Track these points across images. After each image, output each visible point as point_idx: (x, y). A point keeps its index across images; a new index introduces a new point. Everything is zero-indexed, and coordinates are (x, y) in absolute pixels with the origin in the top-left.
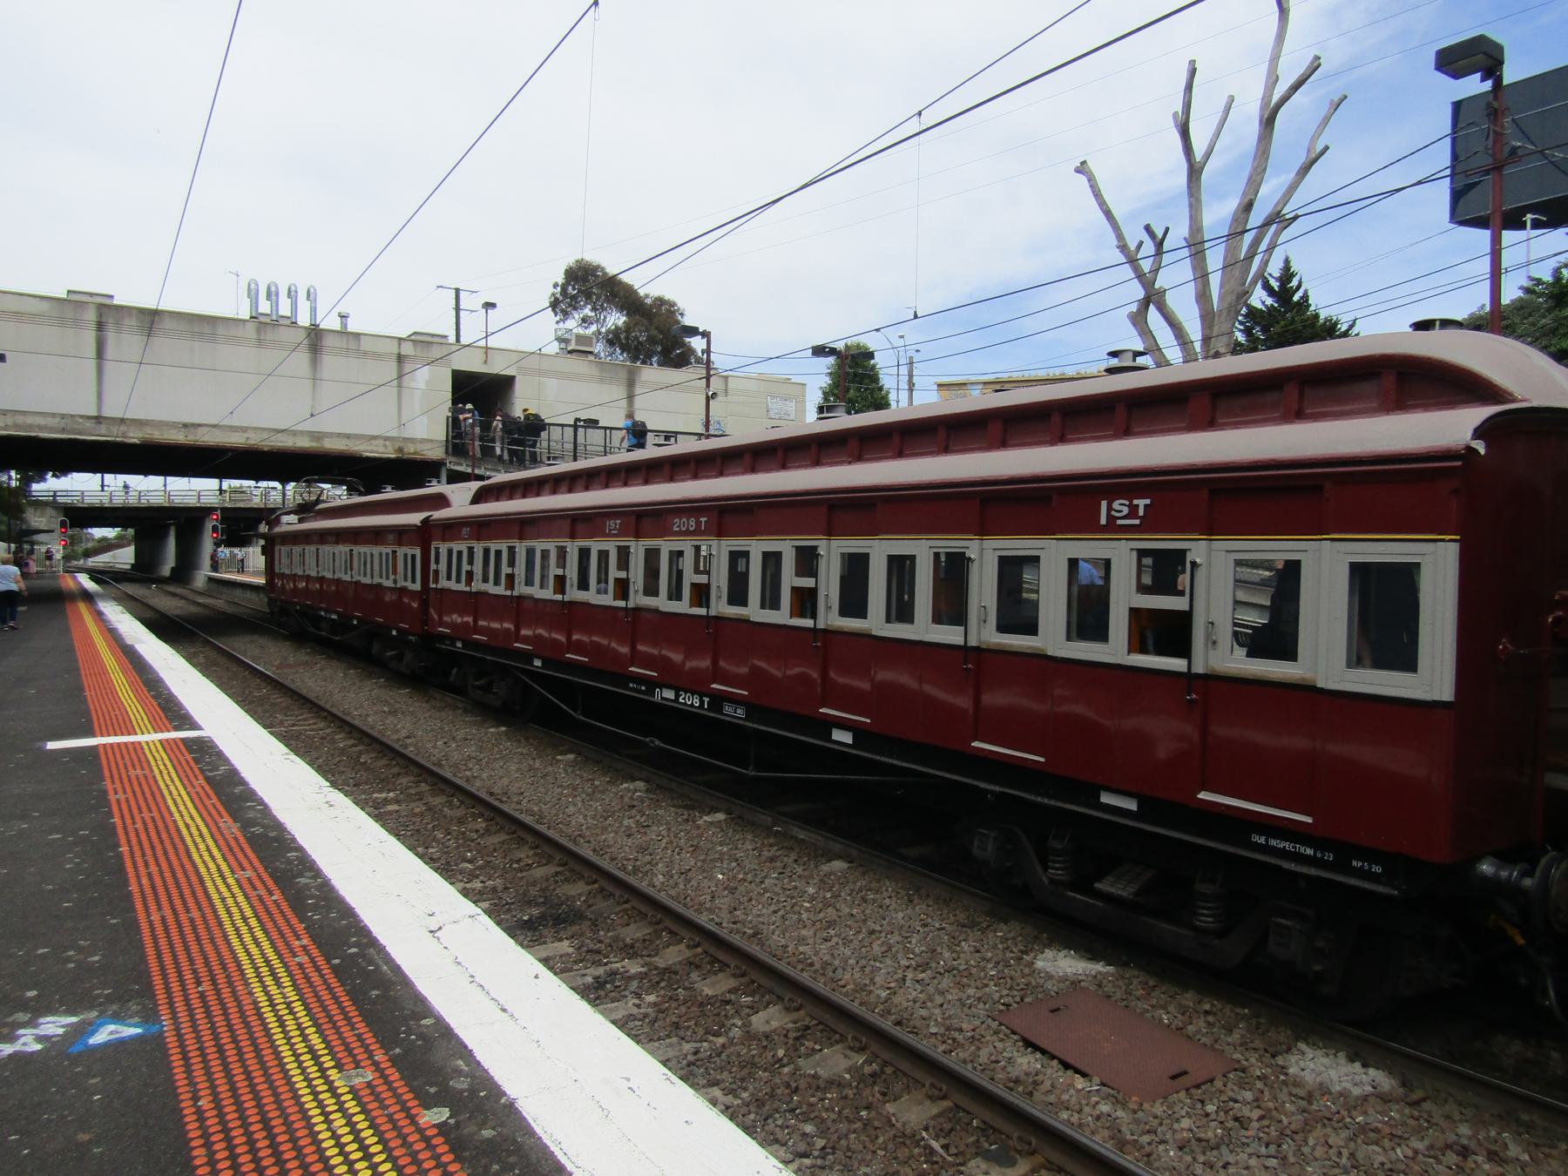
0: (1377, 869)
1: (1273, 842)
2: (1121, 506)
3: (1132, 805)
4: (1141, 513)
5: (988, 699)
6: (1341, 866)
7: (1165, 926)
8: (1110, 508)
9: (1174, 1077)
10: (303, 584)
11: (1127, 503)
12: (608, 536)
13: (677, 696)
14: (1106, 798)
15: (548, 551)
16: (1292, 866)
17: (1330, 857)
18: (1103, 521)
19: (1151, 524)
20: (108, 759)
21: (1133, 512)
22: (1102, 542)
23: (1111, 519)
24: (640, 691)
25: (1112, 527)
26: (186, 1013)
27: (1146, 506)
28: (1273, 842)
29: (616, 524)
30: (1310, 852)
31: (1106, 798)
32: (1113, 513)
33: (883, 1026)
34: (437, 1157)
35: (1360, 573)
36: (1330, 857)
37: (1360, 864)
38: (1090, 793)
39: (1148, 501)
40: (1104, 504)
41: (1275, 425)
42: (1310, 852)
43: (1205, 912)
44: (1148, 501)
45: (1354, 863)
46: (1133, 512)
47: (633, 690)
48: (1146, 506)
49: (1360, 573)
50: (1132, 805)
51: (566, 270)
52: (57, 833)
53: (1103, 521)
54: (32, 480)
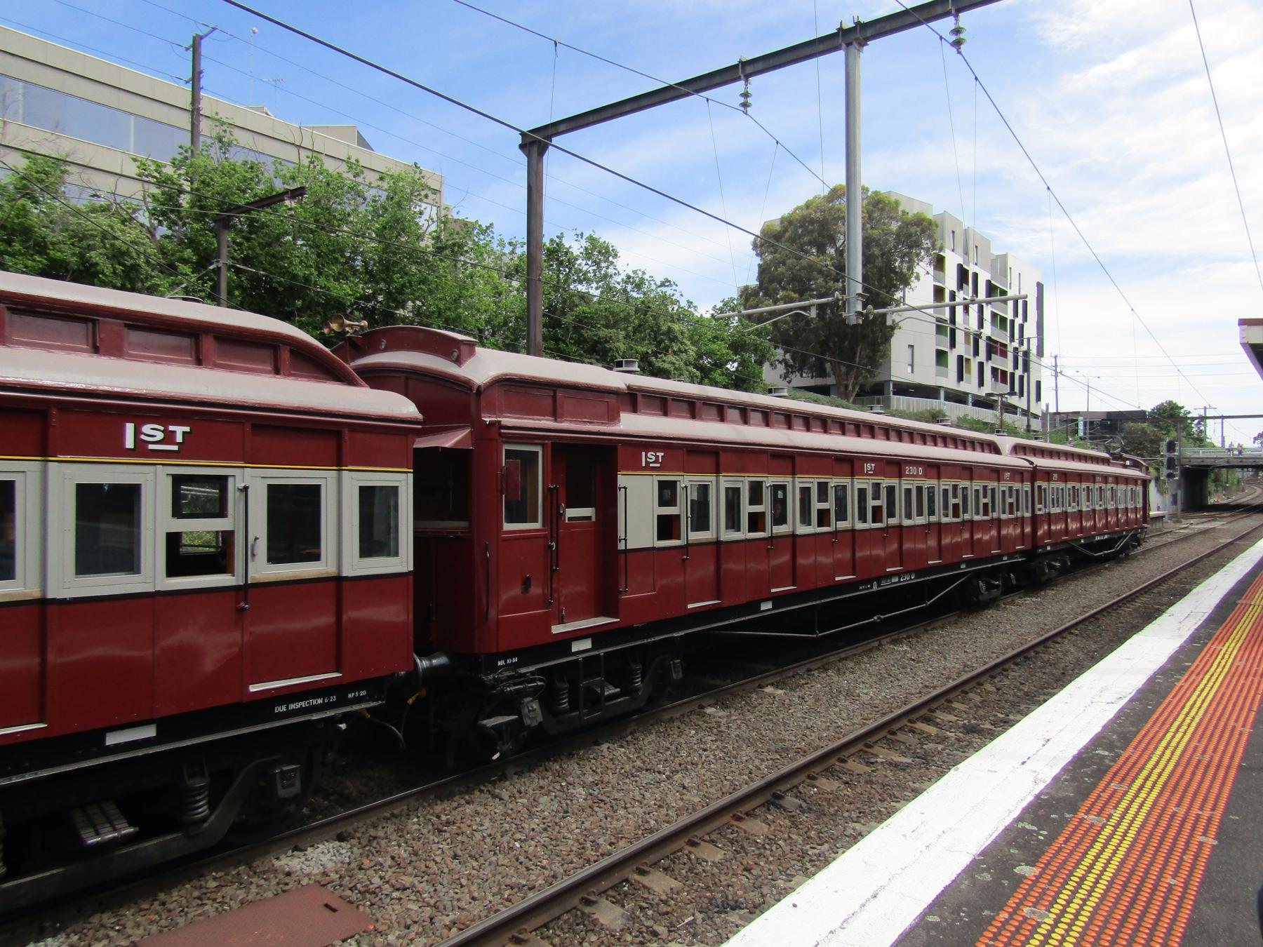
0: (363, 693)
1: (292, 706)
2: (152, 431)
3: (150, 732)
4: (179, 439)
5: (1053, 528)
6: (342, 702)
7: (146, 844)
8: (137, 432)
9: (334, 910)
10: (1073, 526)
11: (162, 428)
12: (645, 469)
13: (287, 708)
14: (112, 739)
15: (893, 487)
16: (315, 717)
17: (333, 699)
18: (644, 465)
19: (188, 450)
20: (1157, 763)
21: (169, 438)
22: (125, 466)
23: (648, 463)
24: (868, 589)
25: (141, 449)
26: (1173, 856)
27: (184, 433)
28: (292, 706)
29: (657, 457)
30: (320, 701)
31: (112, 739)
32: (143, 437)
33: (744, 792)
34: (1011, 915)
35: (276, 493)
36: (333, 699)
37: (353, 694)
38: (92, 741)
39: (187, 429)
40: (644, 453)
41: (157, 360)
42: (320, 701)
43: (201, 803)
44: (187, 429)
45: (350, 696)
46: (169, 438)
47: (863, 590)
48: (184, 433)
49: (276, 493)
50: (150, 732)
51: (1170, 403)
52: (1231, 819)
53: (644, 465)
54: (835, 244)
